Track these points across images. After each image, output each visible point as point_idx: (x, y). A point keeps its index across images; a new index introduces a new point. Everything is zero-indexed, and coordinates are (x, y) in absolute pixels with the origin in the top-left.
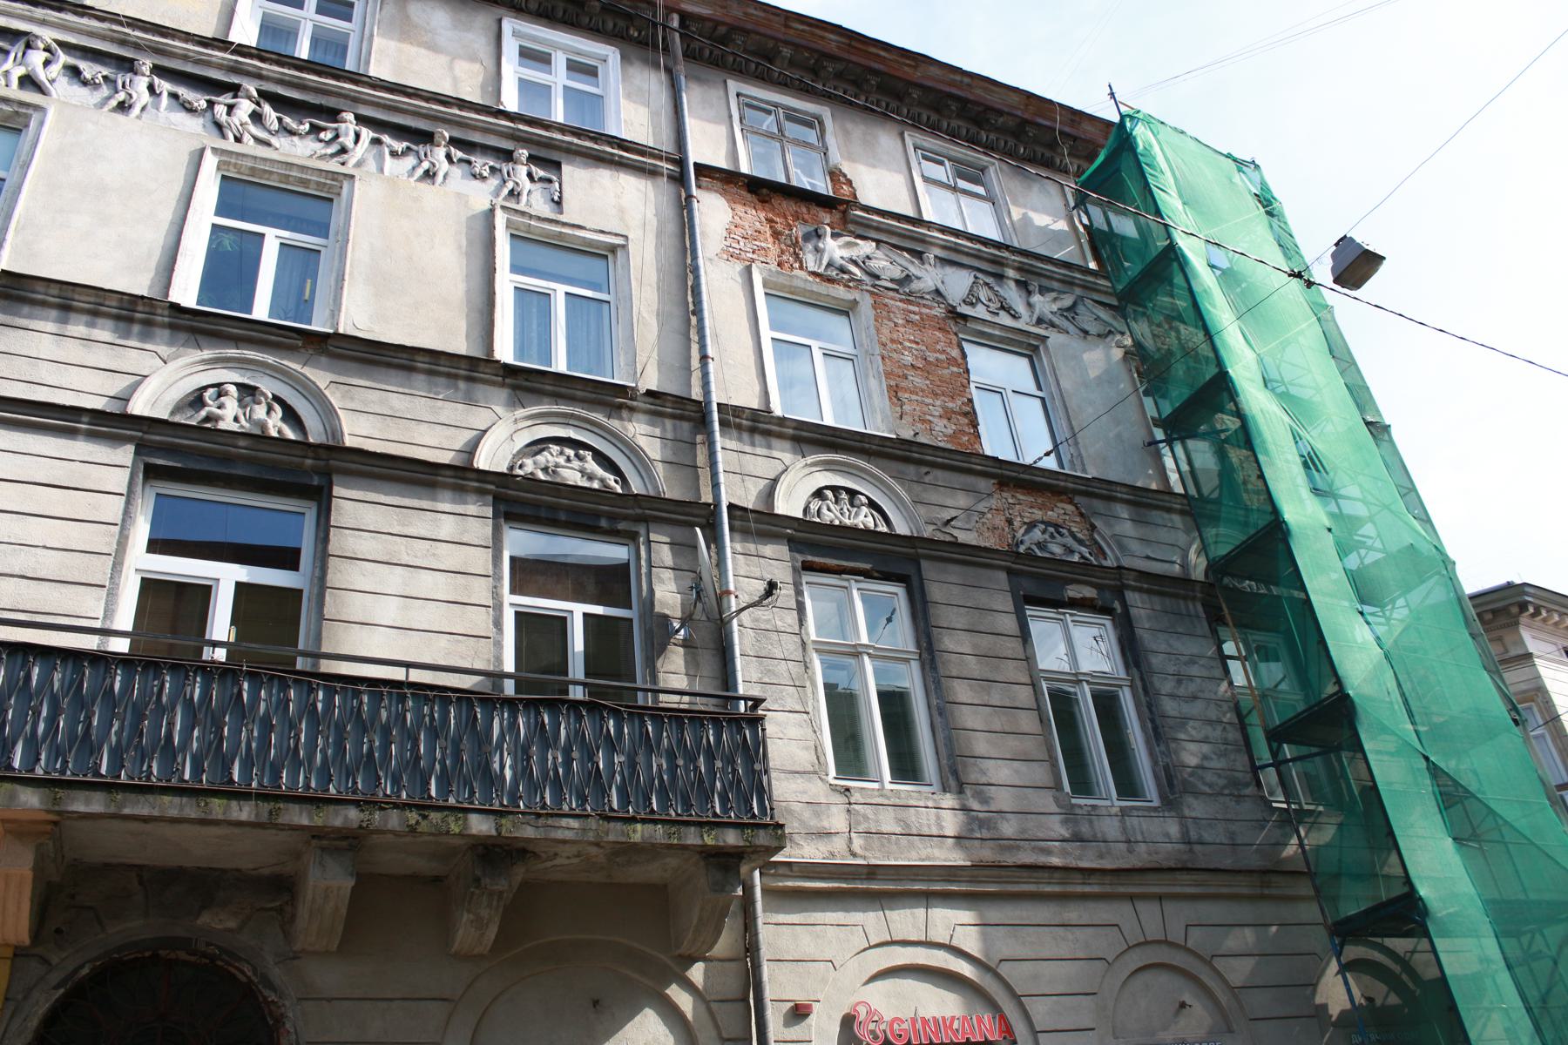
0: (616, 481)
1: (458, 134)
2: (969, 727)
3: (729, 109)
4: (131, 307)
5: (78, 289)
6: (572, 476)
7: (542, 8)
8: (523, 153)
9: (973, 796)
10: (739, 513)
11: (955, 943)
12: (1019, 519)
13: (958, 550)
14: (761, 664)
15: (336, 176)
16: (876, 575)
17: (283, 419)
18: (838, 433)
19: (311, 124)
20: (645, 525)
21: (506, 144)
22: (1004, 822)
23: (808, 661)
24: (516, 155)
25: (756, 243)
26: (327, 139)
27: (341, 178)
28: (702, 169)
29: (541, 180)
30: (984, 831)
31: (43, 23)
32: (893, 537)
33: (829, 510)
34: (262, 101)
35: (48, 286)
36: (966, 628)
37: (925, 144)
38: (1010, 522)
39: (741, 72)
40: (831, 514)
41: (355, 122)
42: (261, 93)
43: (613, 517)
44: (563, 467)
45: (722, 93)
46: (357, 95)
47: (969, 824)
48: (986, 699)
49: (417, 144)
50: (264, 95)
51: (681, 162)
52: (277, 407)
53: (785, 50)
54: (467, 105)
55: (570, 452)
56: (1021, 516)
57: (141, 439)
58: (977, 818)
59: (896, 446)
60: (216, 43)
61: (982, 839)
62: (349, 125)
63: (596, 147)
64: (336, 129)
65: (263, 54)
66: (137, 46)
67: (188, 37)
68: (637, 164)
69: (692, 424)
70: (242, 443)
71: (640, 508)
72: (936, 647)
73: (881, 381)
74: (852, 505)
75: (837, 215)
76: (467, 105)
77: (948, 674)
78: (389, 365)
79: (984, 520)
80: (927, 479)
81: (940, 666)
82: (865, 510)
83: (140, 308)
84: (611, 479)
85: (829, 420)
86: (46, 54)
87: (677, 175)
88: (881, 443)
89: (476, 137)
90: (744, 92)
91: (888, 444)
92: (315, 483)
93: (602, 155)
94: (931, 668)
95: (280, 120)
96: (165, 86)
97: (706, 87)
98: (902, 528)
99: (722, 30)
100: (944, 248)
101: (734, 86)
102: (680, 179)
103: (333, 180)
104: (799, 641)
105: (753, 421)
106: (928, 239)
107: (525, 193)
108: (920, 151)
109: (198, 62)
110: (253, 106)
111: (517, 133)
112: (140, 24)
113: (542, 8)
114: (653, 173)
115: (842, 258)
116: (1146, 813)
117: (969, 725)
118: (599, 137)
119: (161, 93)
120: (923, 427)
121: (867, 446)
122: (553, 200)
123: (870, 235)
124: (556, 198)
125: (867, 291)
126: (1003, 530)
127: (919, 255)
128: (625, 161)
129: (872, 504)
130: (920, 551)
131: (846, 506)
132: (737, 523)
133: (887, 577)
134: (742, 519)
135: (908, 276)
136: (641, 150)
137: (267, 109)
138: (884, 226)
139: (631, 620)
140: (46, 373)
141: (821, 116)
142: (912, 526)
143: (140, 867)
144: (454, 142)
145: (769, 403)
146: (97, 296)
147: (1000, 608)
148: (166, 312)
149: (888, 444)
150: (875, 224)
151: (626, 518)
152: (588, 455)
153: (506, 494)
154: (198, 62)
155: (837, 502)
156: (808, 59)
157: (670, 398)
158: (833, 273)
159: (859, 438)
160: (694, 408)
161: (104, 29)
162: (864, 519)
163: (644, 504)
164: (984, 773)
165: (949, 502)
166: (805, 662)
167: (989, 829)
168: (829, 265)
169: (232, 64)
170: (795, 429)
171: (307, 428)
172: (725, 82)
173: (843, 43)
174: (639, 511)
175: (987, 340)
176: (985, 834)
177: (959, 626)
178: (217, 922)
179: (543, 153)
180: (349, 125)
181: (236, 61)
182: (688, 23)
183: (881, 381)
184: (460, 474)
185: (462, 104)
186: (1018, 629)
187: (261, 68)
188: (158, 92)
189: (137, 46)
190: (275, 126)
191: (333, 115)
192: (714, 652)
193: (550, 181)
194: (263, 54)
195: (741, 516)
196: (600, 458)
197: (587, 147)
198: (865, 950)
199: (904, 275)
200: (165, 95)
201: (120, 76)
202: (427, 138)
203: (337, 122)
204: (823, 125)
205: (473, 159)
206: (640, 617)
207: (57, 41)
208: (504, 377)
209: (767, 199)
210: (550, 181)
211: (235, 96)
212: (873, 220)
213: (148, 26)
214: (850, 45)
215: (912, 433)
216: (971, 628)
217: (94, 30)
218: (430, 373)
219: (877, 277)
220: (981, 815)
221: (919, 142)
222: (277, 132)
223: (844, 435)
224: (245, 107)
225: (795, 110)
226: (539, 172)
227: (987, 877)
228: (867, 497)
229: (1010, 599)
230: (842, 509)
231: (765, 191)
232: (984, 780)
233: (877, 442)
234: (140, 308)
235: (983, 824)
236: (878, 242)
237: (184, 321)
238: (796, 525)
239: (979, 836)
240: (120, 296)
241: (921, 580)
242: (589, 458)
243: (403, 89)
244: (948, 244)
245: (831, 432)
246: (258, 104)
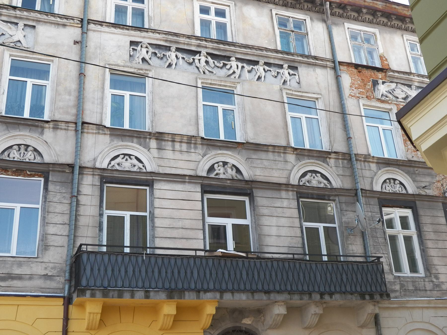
0: (328, 183)
1: (266, 61)
2: (432, 256)
3: (346, 35)
4: (190, 139)
5: (176, 135)
6: (314, 183)
7: (284, 3)
8: (286, 66)
9: (434, 278)
10: (364, 191)
11: (430, 322)
12: (445, 183)
13: (427, 197)
14: (373, 239)
15: (235, 83)
16: (403, 207)
17: (236, 172)
18: (390, 160)
19: (223, 63)
20: (338, 197)
21: (281, 63)
22: (444, 285)
23: (386, 237)
24: (284, 66)
25: (360, 90)
26: (228, 68)
27: (236, 84)
28: (340, 63)
29: (292, 74)
30: (438, 288)
31: (144, 37)
32: (407, 194)
33: (388, 187)
34: (208, 56)
35: (168, 135)
36: (430, 223)
37: (410, 39)
38: (442, 185)
39: (348, 18)
40: (389, 189)
41: (235, 60)
42: (207, 53)
43: (329, 196)
44: (313, 180)
45: (343, 28)
46: (235, 51)
47: (433, 286)
48: (436, 246)
49: (254, 66)
50: (208, 54)
51: (334, 62)
52: (234, 169)
53: (364, 11)
54: (268, 50)
55: (314, 175)
56: (446, 182)
57: (202, 183)
58: (435, 284)
59: (407, 162)
60: (192, 37)
61: (437, 291)
62: (233, 63)
63: (308, 60)
64: (231, 64)
65: (206, 39)
66: (171, 42)
67: (184, 35)
68: (321, 65)
69: (347, 161)
70: (228, 182)
71: (336, 192)
72: (422, 230)
73: (401, 139)
74: (395, 184)
75: (383, 74)
76: (268, 50)
77: (426, 239)
78: (262, 151)
79: (434, 185)
80: (417, 172)
81: (423, 236)
82: (398, 185)
83: (193, 139)
84: (326, 182)
85: (386, 156)
86: (147, 49)
87: (333, 67)
88: (403, 162)
89: (272, 61)
90: (349, 27)
91: (405, 162)
92: (249, 192)
93: (310, 63)
94: (420, 237)
95: (214, 62)
96: (180, 55)
97: (338, 27)
98: (410, 191)
99: (343, 5)
100: (419, 82)
101: (347, 25)
102: (334, 68)
103: (234, 84)
104: (383, 231)
105: (365, 158)
106: (413, 80)
107: (288, 81)
108: (408, 41)
109: (188, 44)
110: (206, 59)
111: (284, 58)
112: (170, 33)
113: (284, 3)
114: (325, 67)
115: (386, 91)
116: (4, 141)
117: (432, 255)
118: (308, 57)
119: (179, 58)
120: (415, 153)
121: (399, 163)
122: (297, 82)
123: (394, 81)
124: (298, 82)
125: (395, 104)
126: (440, 188)
127: (410, 86)
128: (317, 64)
129: (401, 183)
130: (416, 199)
131: (392, 184)
132: (363, 195)
133: (406, 207)
134: (364, 193)
135: (407, 95)
136: (322, 59)
137: (210, 59)
138: (399, 77)
139: (336, 227)
140: (172, 164)
141: (375, 33)
142: (413, 189)
143: (227, 308)
144: (266, 64)
145: (369, 151)
146: (181, 137)
147: (441, 216)
148: (200, 140)
149: (405, 162)
150: (396, 77)
151: (332, 195)
152: (319, 175)
153: (300, 191)
154: (188, 44)
155: (390, 184)
156: (372, 12)
157: (341, 153)
158: (383, 98)
159: (396, 161)
160: (347, 156)
161: (161, 37)
162: (398, 189)
163: (337, 191)
164: (437, 270)
165: (424, 180)
166: (385, 238)
167: (439, 288)
168: (382, 95)
169: (198, 44)
170: (377, 160)
171: (243, 174)
172: (344, 24)
173: (383, 5)
174: (336, 193)
175: (434, 26)
176: (438, 289)
177: (428, 223)
178: (247, 321)
179: (292, 64)
180: (233, 63)
181: (199, 43)
182: (332, 4)
183: (401, 139)
184: (287, 186)
185: (267, 50)
186: (446, 222)
187: (206, 45)
188: (178, 58)
189: (171, 42)
190: (213, 66)
191: (228, 58)
192: (360, 237)
193: (295, 75)
194: (206, 39)
195: (364, 192)
196: (323, 176)
197: (305, 61)
198: (406, 324)
199: (406, 96)
200: (181, 58)
201: (167, 53)
202: (256, 63)
203: (230, 61)
204: (376, 36)
205: (271, 70)
206: (339, 227)
207: (149, 44)
208: (293, 151)
209: (361, 71)
210: (295, 75)
211: (200, 56)
212: (395, 75)
213: (172, 34)
214: (386, 6)
215: (411, 156)
216: (431, 223)
217: (158, 38)
218: (273, 152)
219: (397, 98)
220: (436, 283)
221: (408, 38)
222: (214, 67)
223: (392, 160)
224: (203, 59)
225: (367, 31)
226: (292, 72)
227: (439, 302)
228: (399, 181)
229: (443, 212)
230: (392, 186)
231: (360, 68)
232: (437, 272)
233: (402, 162)
234: (193, 139)
235: (438, 286)
236: (397, 83)
237: (205, 142)
238: (380, 193)
239: (436, 290)
240: (187, 136)
241: (416, 208)
242: (320, 176)
243: (248, 46)
244: (420, 81)
245: (388, 160)
246: (207, 57)
